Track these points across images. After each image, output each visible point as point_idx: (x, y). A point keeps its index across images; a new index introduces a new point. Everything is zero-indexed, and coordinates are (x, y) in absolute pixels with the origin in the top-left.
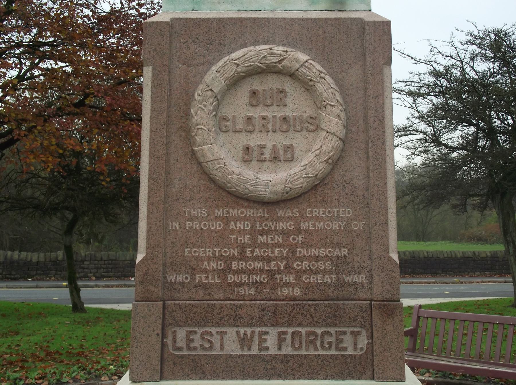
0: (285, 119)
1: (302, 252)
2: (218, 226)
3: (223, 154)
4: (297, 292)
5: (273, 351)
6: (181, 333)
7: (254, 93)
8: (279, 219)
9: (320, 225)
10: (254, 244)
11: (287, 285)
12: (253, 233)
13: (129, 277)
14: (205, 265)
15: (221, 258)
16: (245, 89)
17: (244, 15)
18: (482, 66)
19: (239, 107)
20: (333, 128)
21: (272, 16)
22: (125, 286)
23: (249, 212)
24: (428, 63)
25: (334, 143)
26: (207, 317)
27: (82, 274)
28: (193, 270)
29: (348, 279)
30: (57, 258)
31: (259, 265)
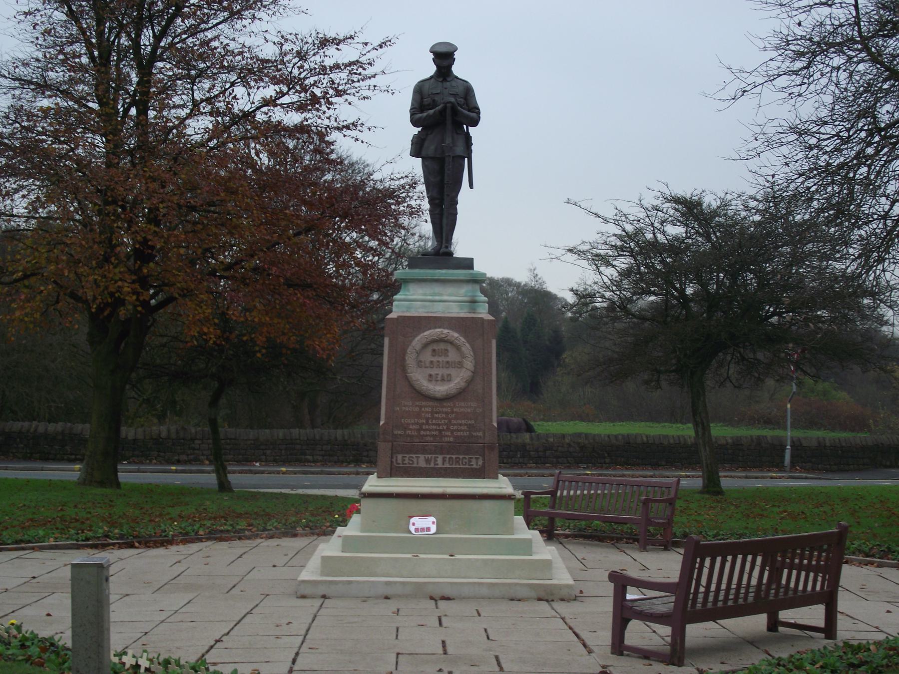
0: (448, 362)
1: (454, 422)
2: (417, 409)
3: (419, 378)
4: (452, 439)
5: (440, 465)
6: (400, 457)
7: (434, 350)
8: (444, 407)
9: (462, 410)
10: (433, 418)
11: (447, 436)
12: (432, 413)
13: (252, 461)
14: (411, 427)
15: (418, 424)
16: (430, 349)
17: (430, 315)
18: (676, 230)
19: (427, 357)
20: (468, 367)
21: (443, 315)
22: (251, 472)
23: (431, 403)
24: (616, 223)
25: (469, 374)
26: (411, 450)
27: (192, 457)
28: (405, 429)
29: (474, 434)
30: (159, 435)
31: (434, 427)
